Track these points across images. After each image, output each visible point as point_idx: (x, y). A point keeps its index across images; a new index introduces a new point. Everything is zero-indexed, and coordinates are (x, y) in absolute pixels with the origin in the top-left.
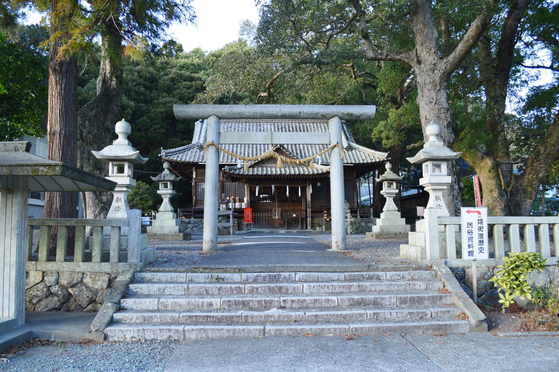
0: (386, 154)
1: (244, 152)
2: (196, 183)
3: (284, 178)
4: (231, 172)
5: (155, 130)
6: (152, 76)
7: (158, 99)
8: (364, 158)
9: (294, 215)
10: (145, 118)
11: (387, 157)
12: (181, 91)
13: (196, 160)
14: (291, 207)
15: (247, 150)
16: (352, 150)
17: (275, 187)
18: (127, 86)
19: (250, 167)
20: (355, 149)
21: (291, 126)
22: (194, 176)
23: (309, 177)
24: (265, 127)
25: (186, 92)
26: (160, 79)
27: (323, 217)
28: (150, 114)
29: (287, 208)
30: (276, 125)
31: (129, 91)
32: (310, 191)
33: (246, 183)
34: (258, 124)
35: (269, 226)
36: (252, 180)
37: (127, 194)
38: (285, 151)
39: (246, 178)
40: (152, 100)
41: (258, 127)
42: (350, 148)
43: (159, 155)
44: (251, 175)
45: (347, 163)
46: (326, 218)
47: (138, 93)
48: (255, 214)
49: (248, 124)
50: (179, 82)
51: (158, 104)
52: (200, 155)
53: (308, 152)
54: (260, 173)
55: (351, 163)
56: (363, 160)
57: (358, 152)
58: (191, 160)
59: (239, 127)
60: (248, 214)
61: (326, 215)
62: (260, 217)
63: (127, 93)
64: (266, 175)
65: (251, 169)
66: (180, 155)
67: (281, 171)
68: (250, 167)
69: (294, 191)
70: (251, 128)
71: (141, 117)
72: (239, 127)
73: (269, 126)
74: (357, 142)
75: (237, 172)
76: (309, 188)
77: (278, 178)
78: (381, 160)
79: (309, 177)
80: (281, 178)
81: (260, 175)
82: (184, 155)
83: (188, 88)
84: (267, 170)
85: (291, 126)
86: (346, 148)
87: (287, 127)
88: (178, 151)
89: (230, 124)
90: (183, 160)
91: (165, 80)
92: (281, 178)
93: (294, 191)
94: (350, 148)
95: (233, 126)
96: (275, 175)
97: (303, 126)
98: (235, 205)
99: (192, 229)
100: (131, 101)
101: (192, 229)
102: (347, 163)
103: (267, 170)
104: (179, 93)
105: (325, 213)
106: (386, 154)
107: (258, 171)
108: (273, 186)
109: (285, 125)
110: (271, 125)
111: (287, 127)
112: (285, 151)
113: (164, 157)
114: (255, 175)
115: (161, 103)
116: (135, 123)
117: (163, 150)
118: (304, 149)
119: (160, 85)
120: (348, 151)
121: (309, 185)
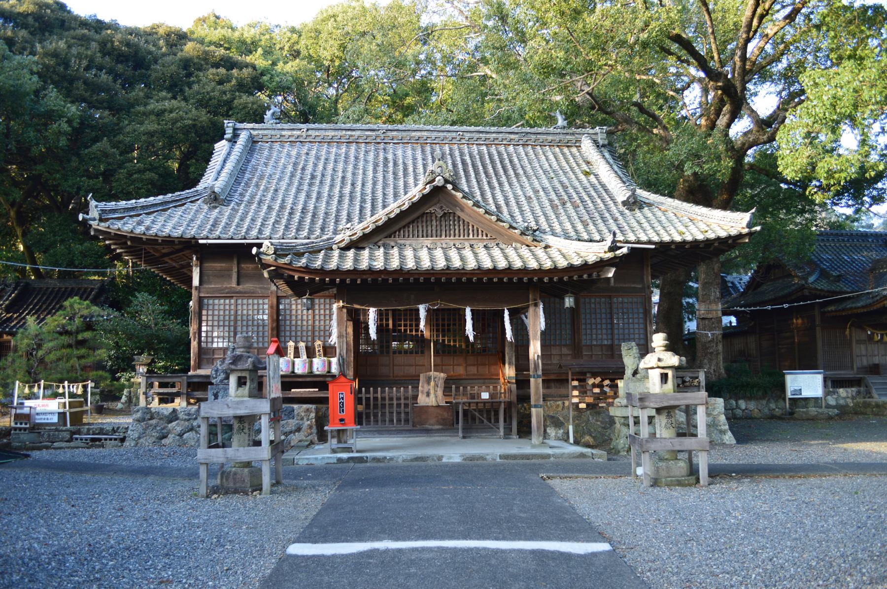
0: (746, 217)
1: (338, 211)
2: (200, 300)
3: (459, 280)
4: (282, 261)
5: (130, 175)
6: (136, 53)
7: (145, 105)
8: (683, 230)
9: (485, 396)
10: (104, 144)
11: (749, 225)
12: (203, 87)
13: (192, 232)
14: (473, 370)
15: (346, 206)
16: (641, 208)
17: (428, 311)
18: (66, 69)
19: (347, 248)
20: (650, 205)
21: (466, 151)
22: (196, 282)
23: (541, 280)
24: (400, 153)
25: (213, 90)
26: (156, 62)
27: (567, 396)
28: (121, 137)
29: (460, 370)
30: (428, 149)
31: (72, 80)
32: (537, 321)
33: (337, 298)
34: (382, 146)
35: (410, 427)
36: (356, 288)
37: (853, 329)
38: (459, 195)
39: (333, 281)
40: (132, 106)
41: (381, 155)
42: (633, 204)
43: (81, 217)
44: (348, 272)
45: (639, 242)
46: (575, 400)
47: (93, 87)
48: (368, 392)
49: (353, 147)
50: (200, 70)
51: (144, 114)
52: (207, 219)
53: (522, 212)
54: (379, 265)
55: (650, 242)
56: (681, 233)
57: (659, 214)
58: (177, 233)
59: (328, 153)
60: (342, 396)
61: (576, 393)
62: (383, 399)
63: (66, 84)
64: (400, 271)
65: (351, 253)
66: (148, 221)
67: (447, 259)
68: (347, 248)
69: (488, 323)
70: (362, 156)
71: (96, 140)
72: (328, 153)
73: (409, 152)
74: (651, 186)
75: (303, 261)
76: (536, 315)
77: (438, 280)
78: (734, 232)
79: (541, 280)
80: (449, 280)
81: (380, 272)
82: (161, 219)
83: (220, 83)
84: (402, 256)
85: (466, 151)
86: (624, 203)
87: (457, 153)
88: (143, 208)
89: (307, 146)
90: (153, 231)
91: (167, 67)
92: (449, 280)
93: (488, 323)
94: (633, 204)
95: (314, 152)
96: (431, 272)
97: (499, 153)
98: (311, 364)
99: (181, 435)
100: (72, 102)
101: (181, 435)
102: (639, 242)
103: (402, 256)
104: (198, 93)
105: (575, 388)
106: (746, 217)
107: (374, 259)
108: (422, 310)
109: (451, 150)
110: (413, 149)
111: (457, 153)
112: (459, 195)
113: (94, 224)
114: (364, 272)
115: (152, 112)
116: (78, 155)
117: (93, 203)
118: (507, 204)
119: (154, 75)
120: (631, 210)
121: (536, 305)
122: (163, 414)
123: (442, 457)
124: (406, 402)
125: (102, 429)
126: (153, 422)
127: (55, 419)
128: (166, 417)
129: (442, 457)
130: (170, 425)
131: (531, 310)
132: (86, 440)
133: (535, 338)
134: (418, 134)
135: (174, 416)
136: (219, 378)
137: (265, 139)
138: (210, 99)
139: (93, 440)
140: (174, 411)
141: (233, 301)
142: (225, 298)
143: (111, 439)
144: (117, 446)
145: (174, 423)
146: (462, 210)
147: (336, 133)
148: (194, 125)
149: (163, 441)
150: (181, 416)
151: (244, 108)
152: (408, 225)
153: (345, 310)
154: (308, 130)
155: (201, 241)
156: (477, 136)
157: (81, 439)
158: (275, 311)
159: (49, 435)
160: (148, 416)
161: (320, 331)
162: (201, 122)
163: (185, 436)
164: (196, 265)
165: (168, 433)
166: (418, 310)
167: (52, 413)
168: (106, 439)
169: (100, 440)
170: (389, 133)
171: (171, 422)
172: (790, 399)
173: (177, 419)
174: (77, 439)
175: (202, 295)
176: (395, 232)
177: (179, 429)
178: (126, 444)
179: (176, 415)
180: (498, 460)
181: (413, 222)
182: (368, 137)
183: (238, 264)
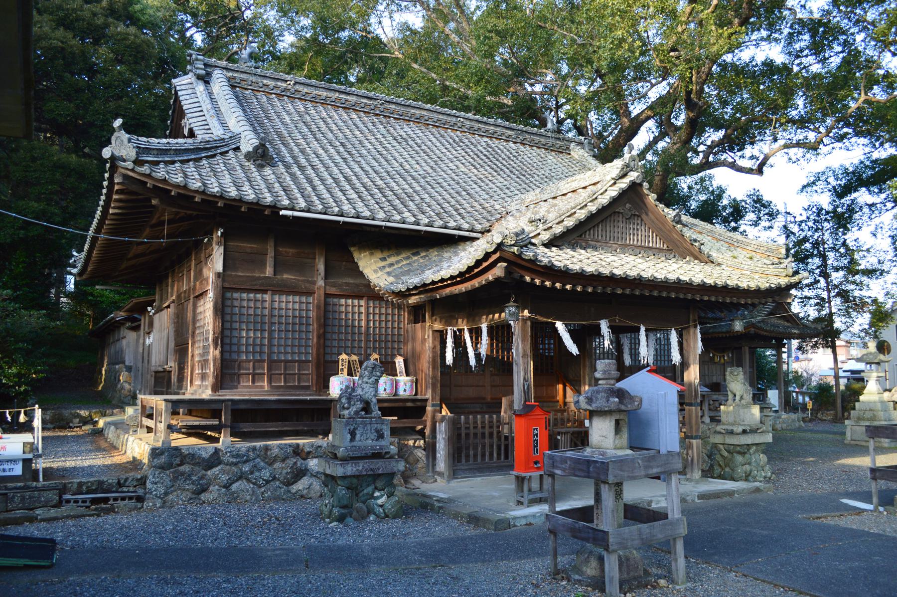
76: (695, 334)
99: (227, 486)
101: (227, 486)
121: (695, 327)
122: (200, 457)
123: (651, 501)
124: (476, 431)
125: (101, 483)
126: (186, 468)
127: (18, 470)
128: (204, 460)
129: (651, 501)
130: (209, 473)
131: (692, 330)
132: (84, 501)
133: (694, 363)
134: (418, 112)
135: (215, 459)
136: (353, 409)
137: (243, 84)
138: (77, 20)
139: (94, 501)
140: (217, 451)
141: (363, 303)
142: (257, 291)
143: (123, 499)
144: (136, 508)
145: (216, 470)
146: (647, 215)
147: (328, 94)
148: (63, 49)
149: (203, 497)
150: (226, 458)
151: (124, 39)
152: (598, 225)
153: (529, 323)
154: (296, 83)
155: (282, 212)
156: (477, 125)
157: (76, 501)
158: (322, 313)
159: (23, 498)
160: (178, 461)
161: (375, 341)
162: (71, 47)
163: (234, 487)
164: (219, 243)
165: (208, 485)
166: (599, 325)
167: (13, 461)
168: (115, 499)
169: (106, 500)
170: (387, 106)
171: (210, 467)
172: (216, 388)
173: (219, 464)
174: (68, 501)
175: (227, 285)
176: (589, 230)
177: (224, 478)
178: (148, 504)
179: (219, 458)
180: (697, 500)
181: (602, 221)
182: (366, 104)
183: (275, 246)
